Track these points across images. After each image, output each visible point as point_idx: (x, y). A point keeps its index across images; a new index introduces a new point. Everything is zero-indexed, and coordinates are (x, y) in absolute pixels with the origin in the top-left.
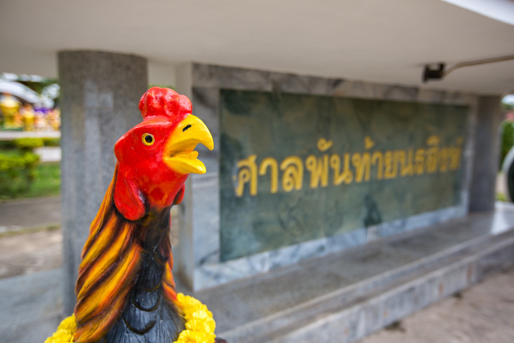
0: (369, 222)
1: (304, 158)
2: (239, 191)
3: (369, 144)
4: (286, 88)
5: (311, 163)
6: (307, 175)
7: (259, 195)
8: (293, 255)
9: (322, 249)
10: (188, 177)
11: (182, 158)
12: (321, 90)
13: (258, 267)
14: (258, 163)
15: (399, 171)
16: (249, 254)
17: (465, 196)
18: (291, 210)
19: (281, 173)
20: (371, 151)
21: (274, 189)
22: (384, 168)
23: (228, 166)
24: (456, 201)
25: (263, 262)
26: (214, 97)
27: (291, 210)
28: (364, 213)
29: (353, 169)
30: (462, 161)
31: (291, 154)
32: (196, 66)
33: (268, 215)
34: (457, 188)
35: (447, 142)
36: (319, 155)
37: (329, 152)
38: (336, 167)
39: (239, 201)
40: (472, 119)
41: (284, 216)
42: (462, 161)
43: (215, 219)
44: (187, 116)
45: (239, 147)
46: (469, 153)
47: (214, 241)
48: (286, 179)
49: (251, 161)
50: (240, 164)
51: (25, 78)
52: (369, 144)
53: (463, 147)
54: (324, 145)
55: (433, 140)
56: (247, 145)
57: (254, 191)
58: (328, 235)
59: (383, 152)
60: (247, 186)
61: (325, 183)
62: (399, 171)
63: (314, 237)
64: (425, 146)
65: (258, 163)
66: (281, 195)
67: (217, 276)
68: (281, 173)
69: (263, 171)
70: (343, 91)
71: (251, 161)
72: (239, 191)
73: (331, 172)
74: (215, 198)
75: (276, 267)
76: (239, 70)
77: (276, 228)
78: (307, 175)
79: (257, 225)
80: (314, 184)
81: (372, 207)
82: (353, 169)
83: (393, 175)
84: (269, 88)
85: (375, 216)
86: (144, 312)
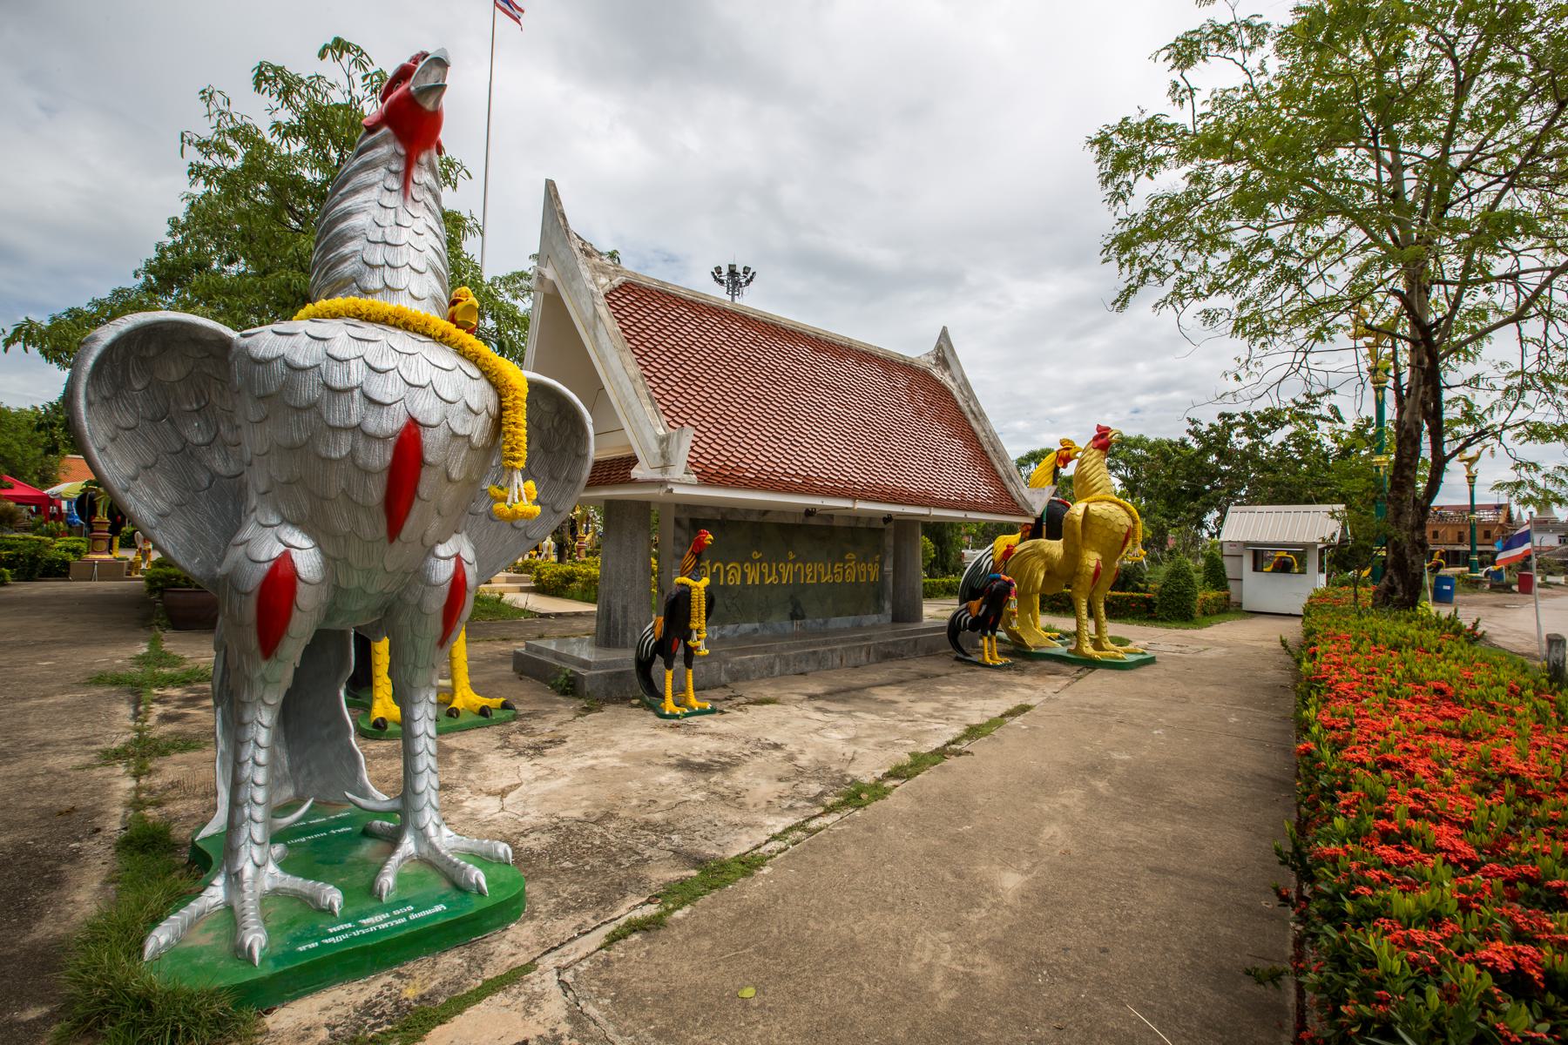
3: (792, 557)
6: (744, 576)
8: (735, 632)
9: (755, 630)
10: (1180, 632)
12: (754, 518)
14: (712, 565)
15: (819, 578)
17: (888, 606)
19: (726, 573)
20: (794, 562)
21: (722, 583)
22: (806, 576)
24: (879, 610)
26: (686, 523)
28: (790, 609)
29: (779, 573)
30: (882, 576)
31: (732, 561)
32: (677, 505)
34: (879, 597)
35: (865, 559)
36: (753, 562)
37: (760, 561)
38: (766, 571)
40: (889, 541)
41: (728, 602)
42: (882, 576)
46: (889, 568)
51: (435, 626)
52: (792, 557)
53: (882, 564)
54: (756, 555)
55: (850, 556)
59: (805, 563)
61: (757, 582)
62: (819, 578)
63: (749, 621)
65: (712, 565)
68: (726, 573)
70: (768, 518)
73: (762, 575)
76: (701, 507)
78: (744, 576)
80: (750, 582)
81: (796, 605)
82: (779, 573)
85: (799, 613)
86: (335, 362)
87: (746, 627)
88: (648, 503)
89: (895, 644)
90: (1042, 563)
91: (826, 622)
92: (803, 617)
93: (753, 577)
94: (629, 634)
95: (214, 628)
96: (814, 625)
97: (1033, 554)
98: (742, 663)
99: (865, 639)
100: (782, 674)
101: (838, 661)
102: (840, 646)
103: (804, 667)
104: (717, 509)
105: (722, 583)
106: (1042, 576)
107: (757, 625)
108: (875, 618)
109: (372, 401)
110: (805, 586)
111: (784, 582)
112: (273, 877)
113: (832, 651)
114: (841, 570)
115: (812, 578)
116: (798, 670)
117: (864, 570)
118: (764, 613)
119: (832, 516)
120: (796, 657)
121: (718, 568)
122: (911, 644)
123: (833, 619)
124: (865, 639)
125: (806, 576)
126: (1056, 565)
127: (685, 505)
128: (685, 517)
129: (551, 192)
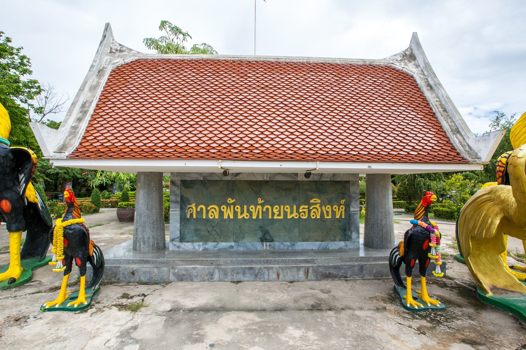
0: (263, 240)
1: (220, 206)
2: (188, 216)
4: (209, 178)
5: (335, 208)
6: (221, 213)
7: (197, 218)
8: (215, 247)
11: (92, 169)
13: (197, 248)
14: (197, 207)
16: (193, 242)
18: (214, 227)
19: (207, 212)
21: (204, 217)
23: (184, 207)
25: (199, 246)
26: (178, 183)
27: (214, 227)
28: (260, 234)
32: (172, 173)
33: (202, 227)
36: (228, 205)
39: (188, 220)
41: (209, 229)
43: (178, 225)
44: (187, 226)
45: (188, 200)
47: (178, 234)
48: (210, 213)
49: (193, 206)
50: (189, 206)
52: (260, 201)
54: (230, 201)
56: (192, 199)
57: (194, 217)
58: (235, 241)
60: (191, 215)
61: (232, 217)
63: (226, 241)
64: (500, 195)
66: (208, 220)
67: (178, 247)
68: (207, 212)
69: (199, 210)
70: (239, 178)
71: (193, 206)
72: (188, 216)
74: (178, 218)
75: (205, 249)
76: (189, 173)
77: (206, 234)
79: (196, 230)
83: (282, 217)
84: (202, 179)
85: (268, 237)
87: (223, 245)
88: (161, 174)
89: (335, 267)
90: (497, 209)
91: (293, 245)
92: (272, 241)
93: (228, 213)
94: (138, 244)
95: (133, 221)
96: (282, 246)
97: (490, 200)
98: (186, 270)
99: (307, 261)
100: (220, 280)
101: (275, 276)
102: (276, 266)
103: (240, 277)
104: (200, 174)
105: (204, 217)
106: (497, 222)
107: (233, 244)
108: (342, 244)
109: (518, 158)
110: (273, 221)
111: (254, 217)
112: (257, 291)
113: (268, 269)
114: (306, 210)
115: (279, 215)
116: (236, 279)
117: (330, 210)
118: (238, 237)
119: (296, 175)
120: (233, 270)
121: (202, 209)
122: (356, 269)
123: (299, 243)
124: (307, 261)
125: (273, 214)
126: (512, 212)
127: (177, 173)
128: (178, 180)
129: (108, 26)
